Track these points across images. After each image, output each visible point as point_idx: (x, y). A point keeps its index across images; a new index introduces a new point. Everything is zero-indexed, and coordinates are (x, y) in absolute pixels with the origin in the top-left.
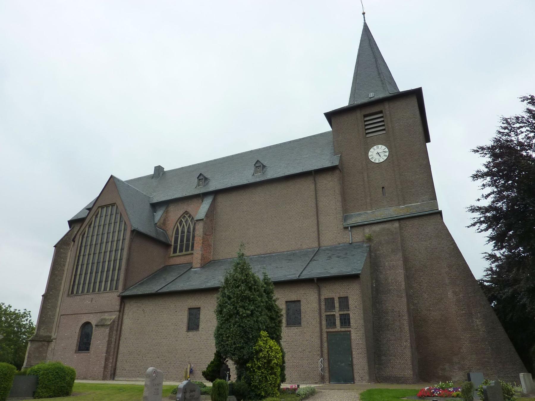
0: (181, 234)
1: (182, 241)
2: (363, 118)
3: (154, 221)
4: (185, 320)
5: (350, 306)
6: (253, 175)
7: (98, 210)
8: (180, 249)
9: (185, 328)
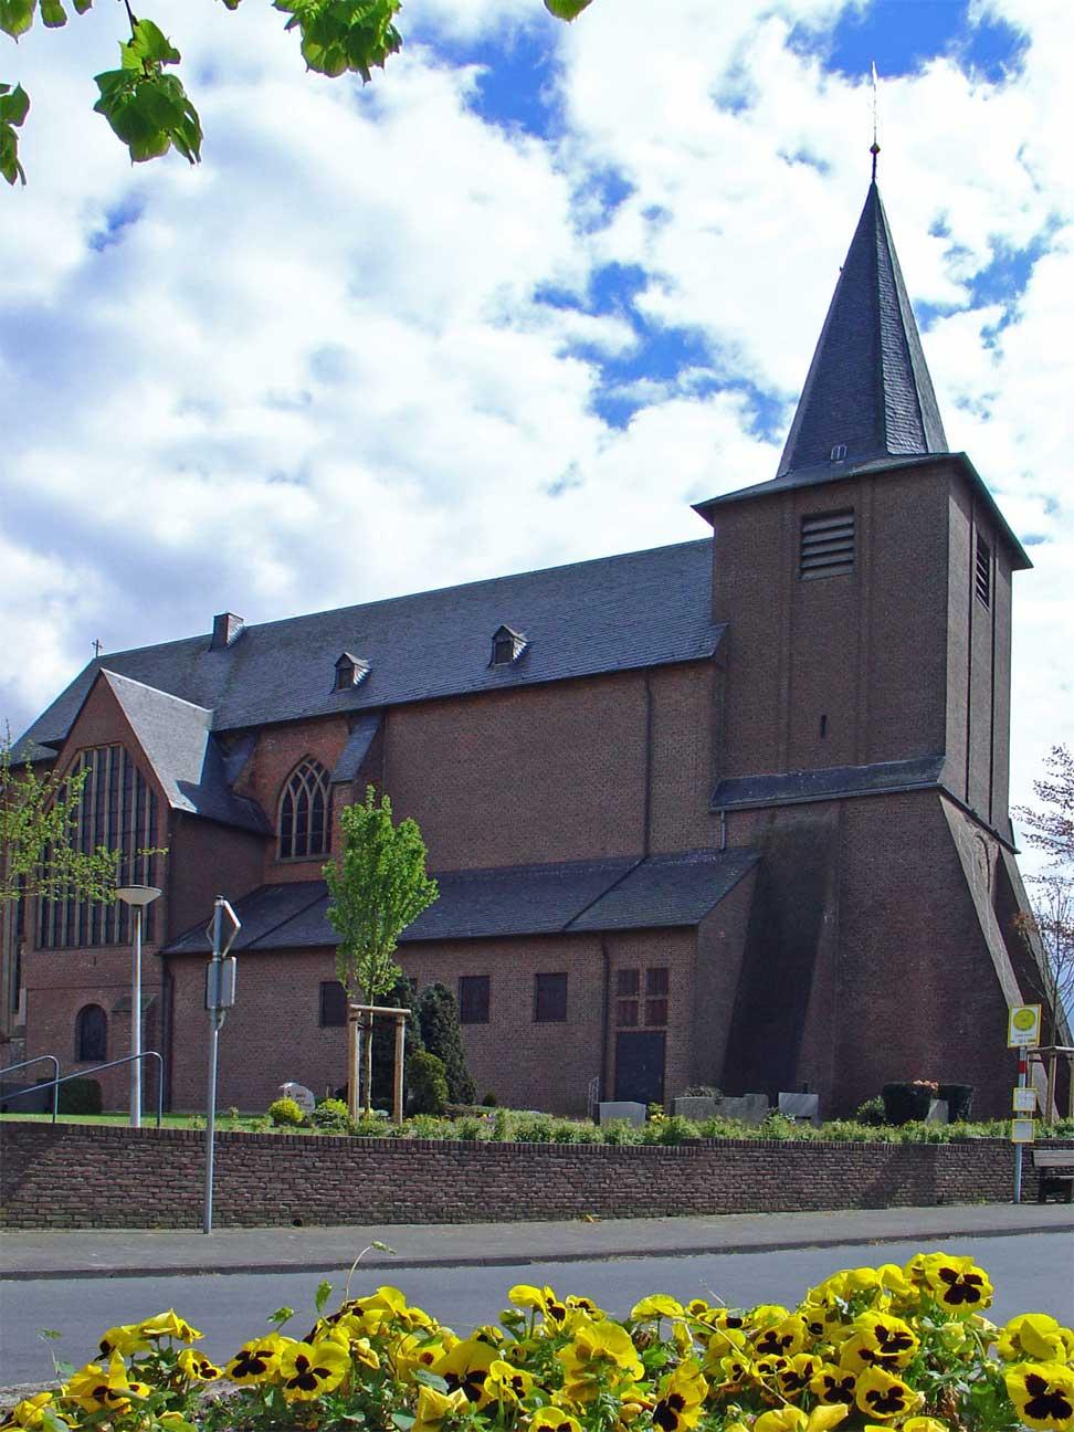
0: (299, 810)
1: (302, 827)
2: (799, 524)
3: (101, 1421)
4: (316, 1005)
5: (671, 986)
6: (489, 666)
7: (77, 756)
8: (313, 824)
9: (316, 1020)
